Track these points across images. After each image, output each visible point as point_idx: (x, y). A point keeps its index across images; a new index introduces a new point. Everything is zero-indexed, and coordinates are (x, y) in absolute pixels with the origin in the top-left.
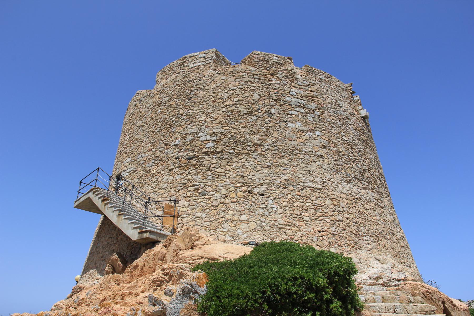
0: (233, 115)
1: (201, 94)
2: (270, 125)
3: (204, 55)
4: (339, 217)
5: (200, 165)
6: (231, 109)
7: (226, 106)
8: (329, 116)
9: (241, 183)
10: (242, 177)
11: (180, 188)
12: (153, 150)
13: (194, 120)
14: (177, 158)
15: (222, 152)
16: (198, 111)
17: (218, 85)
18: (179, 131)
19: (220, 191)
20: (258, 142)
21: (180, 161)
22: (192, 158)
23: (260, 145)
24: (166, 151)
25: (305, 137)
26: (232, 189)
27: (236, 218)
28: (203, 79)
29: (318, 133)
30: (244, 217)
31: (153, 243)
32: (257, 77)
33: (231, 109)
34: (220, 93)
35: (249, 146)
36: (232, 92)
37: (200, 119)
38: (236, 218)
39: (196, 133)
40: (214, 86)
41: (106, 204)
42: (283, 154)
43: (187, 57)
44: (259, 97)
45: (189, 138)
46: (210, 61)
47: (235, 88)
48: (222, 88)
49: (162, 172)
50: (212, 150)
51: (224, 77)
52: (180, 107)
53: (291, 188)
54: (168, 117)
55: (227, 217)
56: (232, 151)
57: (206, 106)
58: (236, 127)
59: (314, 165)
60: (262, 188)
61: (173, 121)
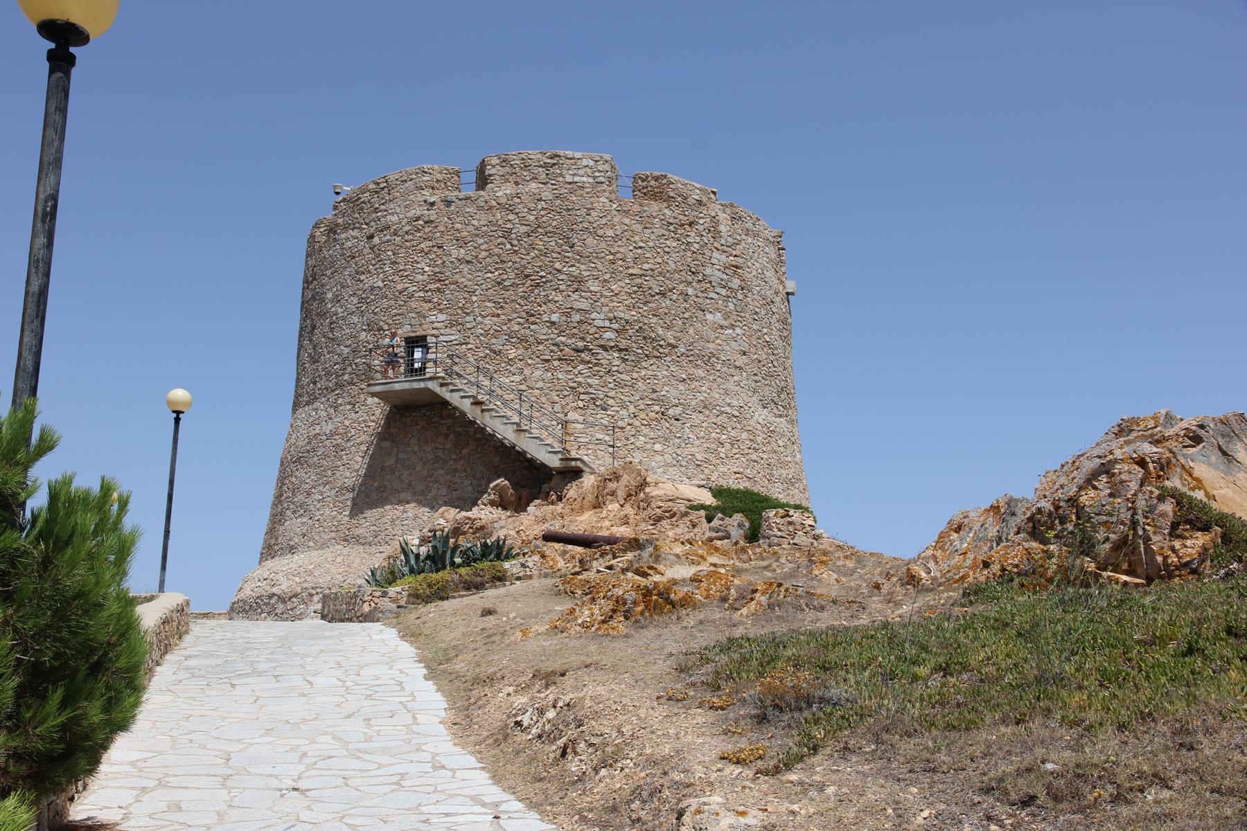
1: (590, 241)
2: (686, 315)
3: (591, 163)
4: (754, 457)
5: (596, 365)
7: (631, 275)
8: (754, 302)
10: (654, 391)
11: (566, 393)
14: (556, 345)
19: (626, 408)
20: (672, 341)
22: (582, 351)
23: (674, 347)
24: (532, 327)
25: (723, 337)
26: (642, 407)
27: (648, 446)
28: (594, 214)
29: (738, 331)
30: (658, 447)
31: (576, 474)
32: (671, 228)
34: (622, 250)
36: (639, 251)
37: (592, 288)
38: (648, 446)
40: (610, 233)
41: (483, 411)
42: (699, 362)
44: (673, 266)
45: (577, 317)
46: (602, 179)
49: (530, 361)
51: (627, 221)
52: (554, 255)
53: (707, 412)
55: (637, 444)
59: (732, 380)
60: (678, 410)
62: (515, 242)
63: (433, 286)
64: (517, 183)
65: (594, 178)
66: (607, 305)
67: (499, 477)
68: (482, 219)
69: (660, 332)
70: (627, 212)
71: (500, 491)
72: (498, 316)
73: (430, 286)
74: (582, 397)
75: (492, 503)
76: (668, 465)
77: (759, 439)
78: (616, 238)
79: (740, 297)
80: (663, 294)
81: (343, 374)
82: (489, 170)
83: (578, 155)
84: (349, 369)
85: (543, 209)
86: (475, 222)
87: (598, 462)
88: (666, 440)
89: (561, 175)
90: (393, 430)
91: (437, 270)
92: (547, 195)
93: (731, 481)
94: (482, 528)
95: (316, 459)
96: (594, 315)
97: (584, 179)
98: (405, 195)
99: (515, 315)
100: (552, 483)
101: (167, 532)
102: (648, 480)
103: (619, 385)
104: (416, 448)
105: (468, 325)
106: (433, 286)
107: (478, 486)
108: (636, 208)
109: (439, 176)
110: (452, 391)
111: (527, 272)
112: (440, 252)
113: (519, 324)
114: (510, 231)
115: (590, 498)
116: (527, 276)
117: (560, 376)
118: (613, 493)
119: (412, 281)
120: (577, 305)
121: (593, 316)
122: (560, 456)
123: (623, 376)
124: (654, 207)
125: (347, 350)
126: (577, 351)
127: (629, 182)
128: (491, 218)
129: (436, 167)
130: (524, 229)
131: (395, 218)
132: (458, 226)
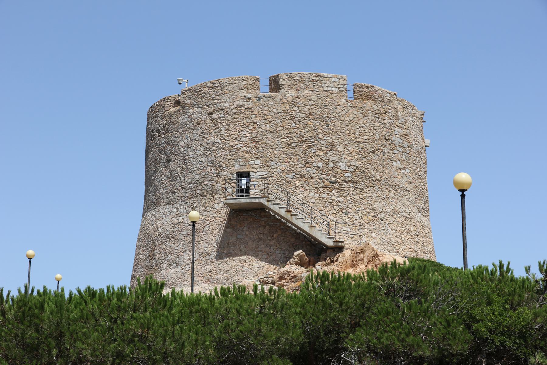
0: (364, 153)
1: (337, 123)
2: (384, 163)
3: (337, 80)
4: (417, 240)
5: (342, 190)
6: (362, 145)
7: (358, 142)
9: (370, 209)
10: (371, 205)
11: (327, 205)
12: (292, 163)
13: (334, 149)
15: (357, 183)
16: (337, 141)
17: (351, 119)
18: (320, 154)
19: (357, 214)
20: (378, 178)
21: (324, 182)
22: (334, 183)
24: (308, 169)
25: (401, 174)
26: (365, 213)
27: (369, 234)
29: (407, 171)
32: (377, 115)
33: (362, 145)
34: (353, 128)
35: (373, 180)
36: (362, 129)
37: (339, 149)
38: (369, 234)
39: (336, 162)
40: (347, 119)
41: (292, 215)
42: (391, 189)
43: (320, 76)
44: (378, 137)
45: (331, 165)
46: (342, 89)
47: (364, 125)
48: (354, 123)
49: (307, 188)
50: (350, 179)
52: (319, 130)
53: (395, 216)
54: (306, 136)
56: (363, 183)
57: (342, 136)
58: (365, 163)
61: (312, 142)
62: (297, 123)
63: (252, 145)
64: (297, 90)
65: (339, 88)
66: (347, 159)
67: (298, 250)
68: (278, 109)
69: (373, 173)
70: (355, 107)
71: (300, 257)
72: (289, 162)
73: (250, 145)
74: (335, 207)
75: (296, 264)
76: (379, 244)
77: (418, 230)
78: (351, 121)
79: (408, 152)
80: (373, 152)
81: (196, 190)
82: (281, 82)
83: (330, 75)
84: (200, 187)
85: (312, 105)
86: (275, 110)
87: (350, 245)
88: (377, 231)
89: (321, 86)
90: (233, 223)
91: (254, 136)
92: (314, 97)
93: (408, 253)
94: (295, 276)
95: (181, 236)
96: (340, 164)
97: (333, 89)
98: (232, 92)
99: (298, 163)
100: (327, 254)
101: (29, 273)
102: (378, 253)
103: (353, 201)
104: (247, 233)
105: (273, 167)
106: (252, 145)
107: (284, 254)
108: (360, 105)
109: (250, 82)
110: (274, 204)
111: (304, 139)
112: (255, 126)
113: (301, 167)
114: (294, 116)
115: (349, 262)
116: (304, 141)
117: (323, 196)
118: (362, 260)
119: (239, 141)
120: (331, 158)
121: (340, 164)
122: (333, 240)
123: (355, 197)
124: (368, 104)
125: (198, 177)
126: (332, 183)
127: (352, 88)
128: (284, 109)
129: (248, 77)
130: (302, 116)
131: (226, 105)
132: (265, 112)
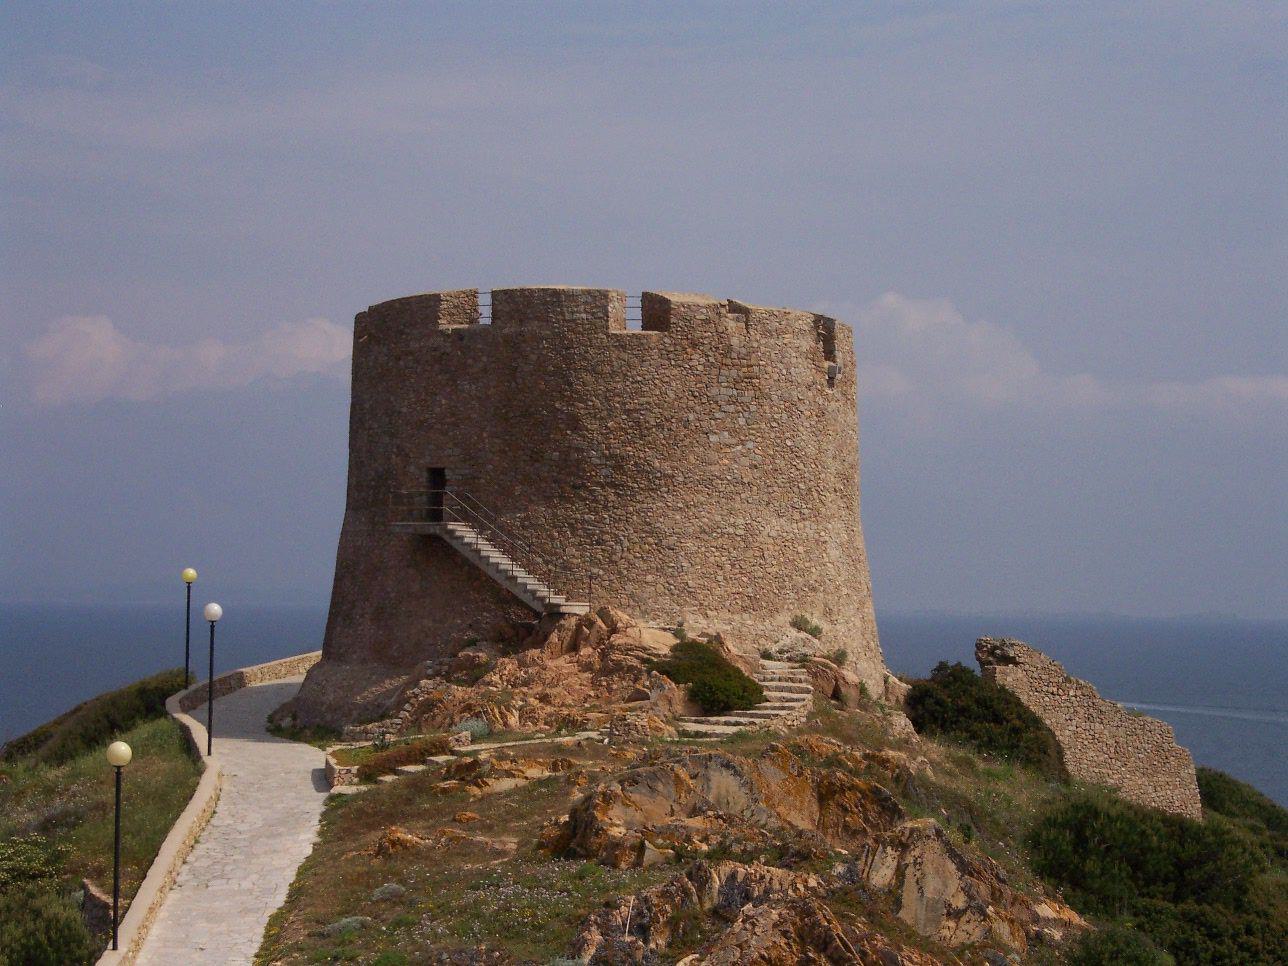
29: (750, 445)
30: (649, 578)
